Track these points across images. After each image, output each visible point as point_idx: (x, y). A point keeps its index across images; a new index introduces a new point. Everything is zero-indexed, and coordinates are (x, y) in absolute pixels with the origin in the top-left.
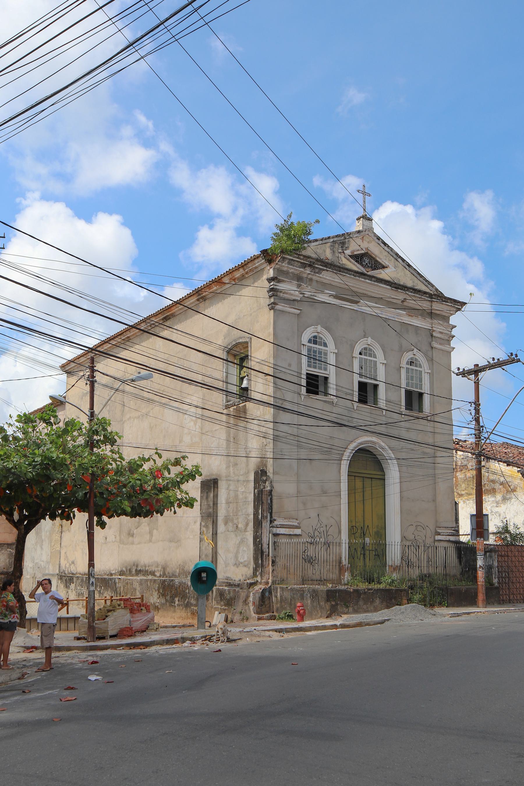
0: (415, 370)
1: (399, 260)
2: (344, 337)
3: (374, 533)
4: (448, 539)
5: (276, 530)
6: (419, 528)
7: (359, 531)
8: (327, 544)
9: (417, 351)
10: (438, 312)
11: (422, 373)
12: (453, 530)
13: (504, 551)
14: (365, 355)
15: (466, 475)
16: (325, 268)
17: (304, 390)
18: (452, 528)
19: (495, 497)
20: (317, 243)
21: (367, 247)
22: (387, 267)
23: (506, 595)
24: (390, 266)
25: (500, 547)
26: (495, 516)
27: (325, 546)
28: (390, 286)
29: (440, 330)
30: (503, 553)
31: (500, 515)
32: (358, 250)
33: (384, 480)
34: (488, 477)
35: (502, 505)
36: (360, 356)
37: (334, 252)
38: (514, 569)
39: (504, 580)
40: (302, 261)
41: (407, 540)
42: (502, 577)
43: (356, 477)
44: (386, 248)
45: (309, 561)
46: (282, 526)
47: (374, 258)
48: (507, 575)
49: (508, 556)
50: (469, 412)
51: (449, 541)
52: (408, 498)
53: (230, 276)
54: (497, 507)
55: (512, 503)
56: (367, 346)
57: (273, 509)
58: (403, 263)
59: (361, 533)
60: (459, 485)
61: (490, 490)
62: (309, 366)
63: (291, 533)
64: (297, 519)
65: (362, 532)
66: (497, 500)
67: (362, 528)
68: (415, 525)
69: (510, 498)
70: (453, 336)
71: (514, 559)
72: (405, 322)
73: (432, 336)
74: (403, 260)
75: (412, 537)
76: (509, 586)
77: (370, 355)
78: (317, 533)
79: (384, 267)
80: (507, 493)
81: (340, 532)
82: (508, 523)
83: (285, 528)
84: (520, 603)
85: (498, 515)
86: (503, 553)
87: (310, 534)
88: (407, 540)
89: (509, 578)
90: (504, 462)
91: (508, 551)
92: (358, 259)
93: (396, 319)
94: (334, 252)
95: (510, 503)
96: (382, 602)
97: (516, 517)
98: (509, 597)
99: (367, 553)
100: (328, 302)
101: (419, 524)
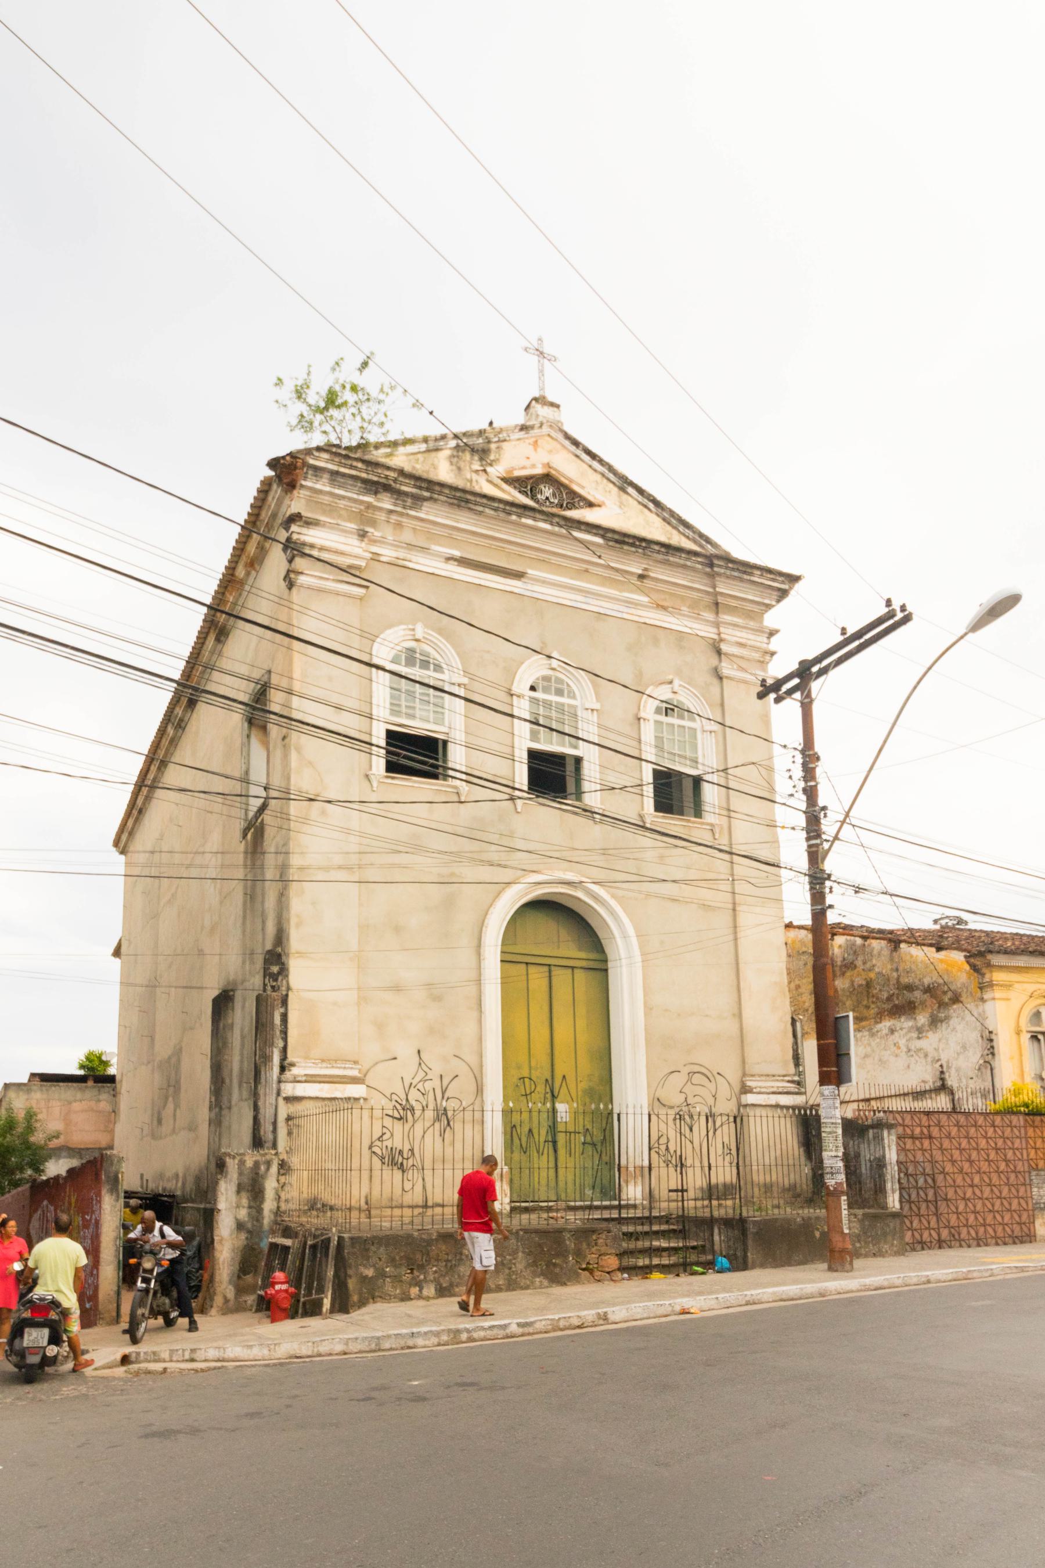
0: (679, 726)
1: (630, 490)
2: (488, 652)
3: (580, 1093)
4: (774, 1103)
5: (294, 1088)
6: (697, 1079)
7: (541, 1088)
8: (442, 1116)
9: (680, 685)
10: (734, 603)
11: (696, 733)
12: (789, 1081)
13: (920, 1126)
14: (546, 690)
15: (852, 982)
16: (426, 494)
17: (379, 764)
18: (784, 1076)
19: (915, 1019)
20: (410, 449)
21: (546, 461)
22: (599, 506)
23: (929, 1228)
24: (607, 502)
25: (908, 1117)
26: (917, 1058)
27: (437, 1125)
28: (603, 537)
29: (741, 640)
30: (917, 1131)
31: (926, 1056)
32: (524, 468)
33: (606, 970)
34: (898, 979)
35: (930, 1034)
36: (533, 694)
37: (459, 469)
38: (949, 1168)
39: (921, 1193)
40: (364, 475)
41: (664, 1105)
42: (917, 1188)
43: (529, 966)
44: (596, 465)
45: (393, 1163)
46: (311, 1079)
47: (566, 487)
48: (930, 1181)
49: (930, 1137)
50: (788, 774)
51: (777, 1106)
52: (666, 1010)
53: (244, 559)
54: (919, 1038)
55: (951, 1027)
56: (551, 672)
57: (289, 1040)
58: (640, 498)
59: (547, 1093)
60: (840, 1004)
61: (903, 1007)
62: (394, 712)
63: (338, 1095)
64: (356, 1062)
65: (548, 1090)
66: (919, 1025)
67: (547, 1080)
68: (685, 1070)
69: (947, 1018)
70: (773, 654)
71: (946, 1144)
72: (648, 621)
73: (719, 652)
74: (640, 491)
75: (678, 1099)
76: (936, 1208)
77: (559, 692)
78: (414, 1095)
79: (591, 505)
80: (939, 1007)
81: (480, 1090)
82: (945, 1069)
83: (320, 1082)
84: (969, 1246)
85: (922, 1055)
86: (917, 1131)
87: (394, 1097)
88: (664, 1105)
89: (935, 1187)
90: (931, 945)
91: (929, 1126)
92: (526, 487)
93: (625, 616)
94: (459, 469)
95: (947, 1029)
96: (803, 1219)
97: (961, 1057)
98: (939, 1235)
99: (561, 1139)
100: (443, 573)
101: (697, 1068)
